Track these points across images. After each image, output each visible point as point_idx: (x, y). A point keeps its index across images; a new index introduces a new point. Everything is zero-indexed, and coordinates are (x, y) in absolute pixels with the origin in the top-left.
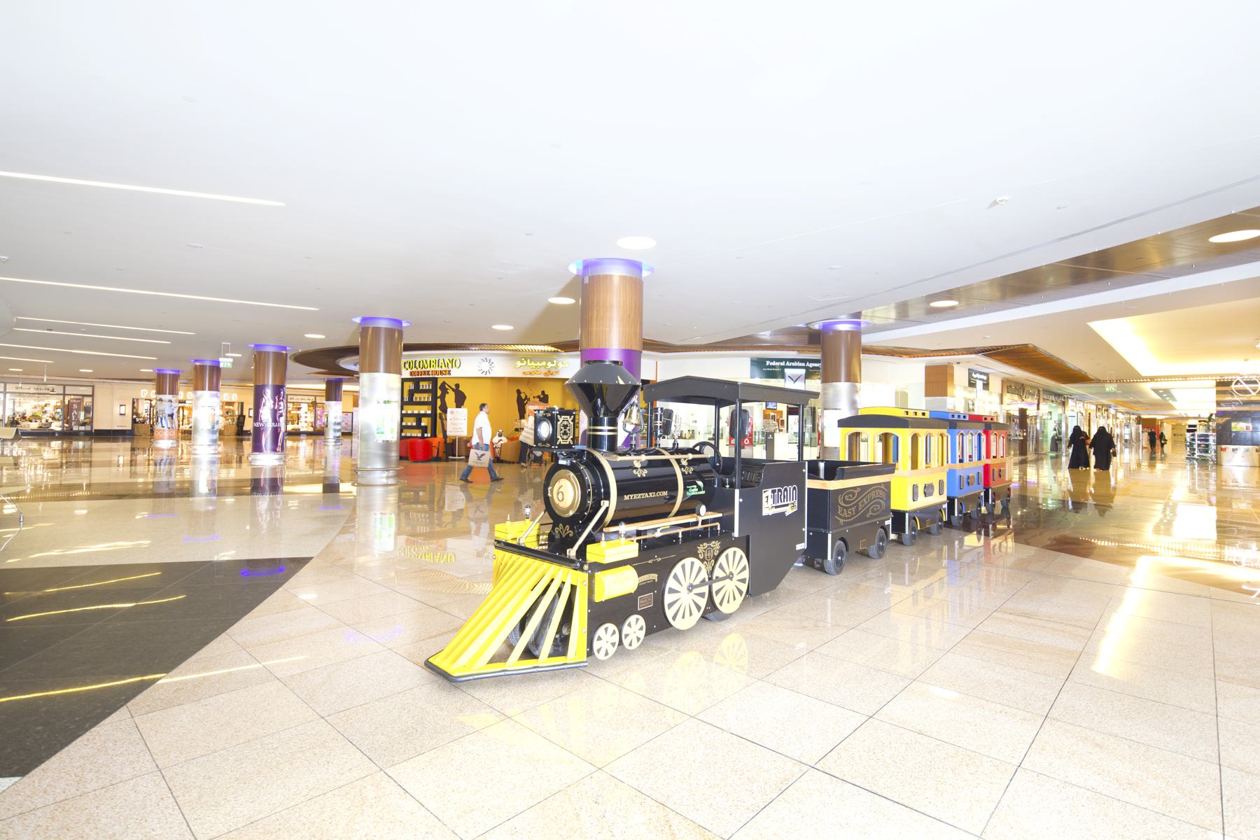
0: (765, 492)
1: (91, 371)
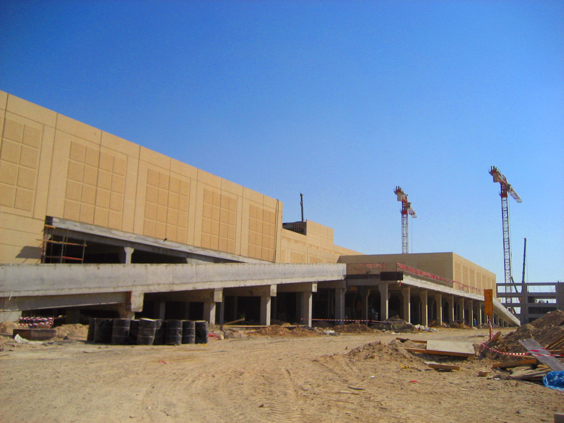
0: (140, 308)
1: (453, 320)
